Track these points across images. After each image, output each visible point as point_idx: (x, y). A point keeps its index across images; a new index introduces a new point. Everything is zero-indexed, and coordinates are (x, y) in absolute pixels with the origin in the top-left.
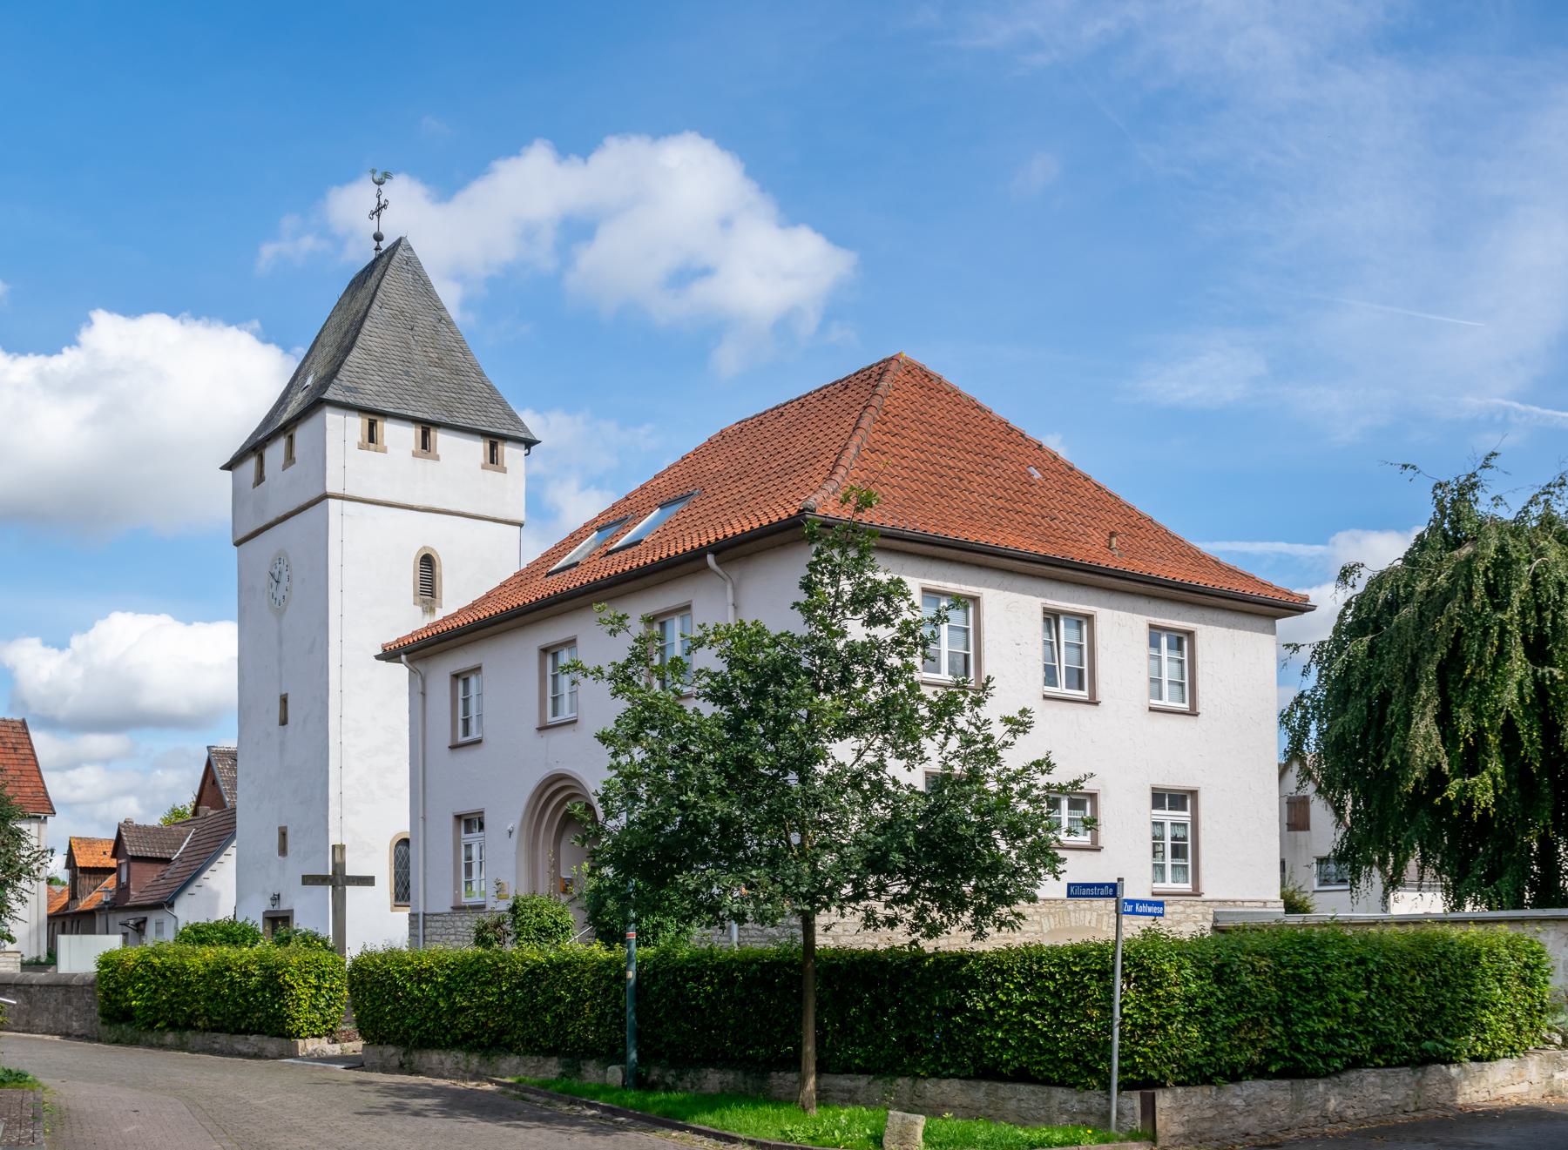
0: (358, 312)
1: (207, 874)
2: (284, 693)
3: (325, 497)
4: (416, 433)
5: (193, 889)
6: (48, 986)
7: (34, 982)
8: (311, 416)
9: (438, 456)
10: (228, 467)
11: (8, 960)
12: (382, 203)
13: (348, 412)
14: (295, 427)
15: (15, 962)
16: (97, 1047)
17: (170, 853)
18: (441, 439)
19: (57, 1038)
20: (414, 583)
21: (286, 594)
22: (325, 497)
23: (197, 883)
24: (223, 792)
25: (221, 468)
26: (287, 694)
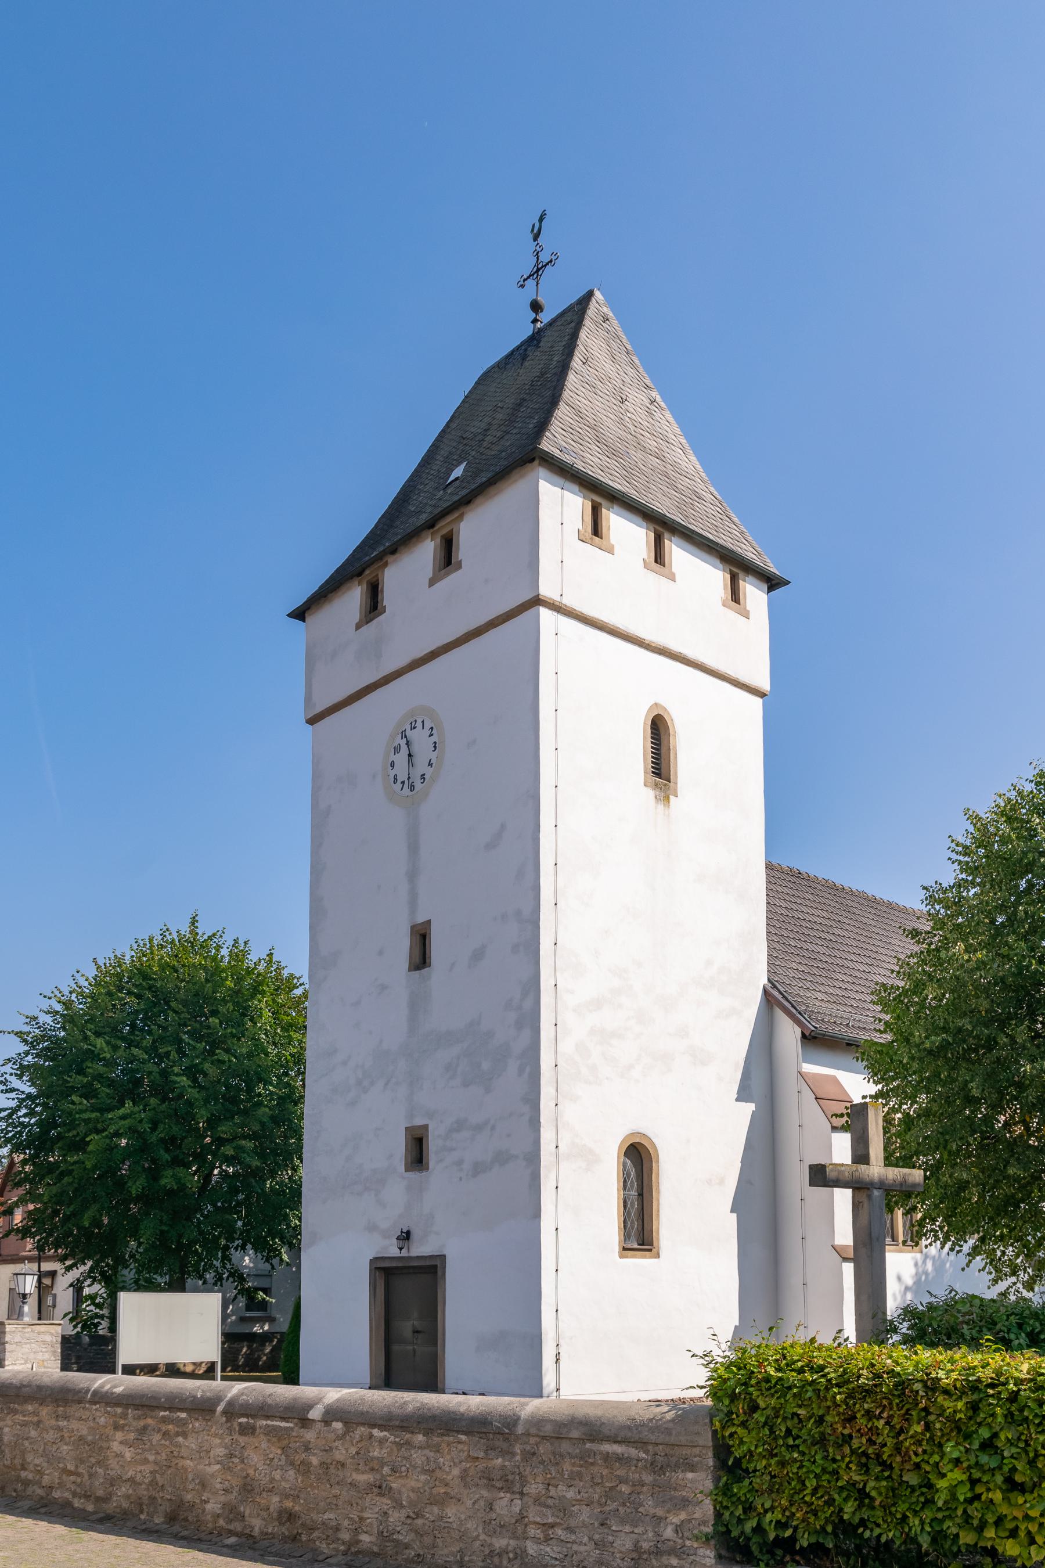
2: (421, 919)
3: (537, 601)
9: (674, 575)
10: (300, 614)
13: (568, 484)
18: (677, 552)
21: (429, 772)
22: (537, 601)
26: (429, 922)
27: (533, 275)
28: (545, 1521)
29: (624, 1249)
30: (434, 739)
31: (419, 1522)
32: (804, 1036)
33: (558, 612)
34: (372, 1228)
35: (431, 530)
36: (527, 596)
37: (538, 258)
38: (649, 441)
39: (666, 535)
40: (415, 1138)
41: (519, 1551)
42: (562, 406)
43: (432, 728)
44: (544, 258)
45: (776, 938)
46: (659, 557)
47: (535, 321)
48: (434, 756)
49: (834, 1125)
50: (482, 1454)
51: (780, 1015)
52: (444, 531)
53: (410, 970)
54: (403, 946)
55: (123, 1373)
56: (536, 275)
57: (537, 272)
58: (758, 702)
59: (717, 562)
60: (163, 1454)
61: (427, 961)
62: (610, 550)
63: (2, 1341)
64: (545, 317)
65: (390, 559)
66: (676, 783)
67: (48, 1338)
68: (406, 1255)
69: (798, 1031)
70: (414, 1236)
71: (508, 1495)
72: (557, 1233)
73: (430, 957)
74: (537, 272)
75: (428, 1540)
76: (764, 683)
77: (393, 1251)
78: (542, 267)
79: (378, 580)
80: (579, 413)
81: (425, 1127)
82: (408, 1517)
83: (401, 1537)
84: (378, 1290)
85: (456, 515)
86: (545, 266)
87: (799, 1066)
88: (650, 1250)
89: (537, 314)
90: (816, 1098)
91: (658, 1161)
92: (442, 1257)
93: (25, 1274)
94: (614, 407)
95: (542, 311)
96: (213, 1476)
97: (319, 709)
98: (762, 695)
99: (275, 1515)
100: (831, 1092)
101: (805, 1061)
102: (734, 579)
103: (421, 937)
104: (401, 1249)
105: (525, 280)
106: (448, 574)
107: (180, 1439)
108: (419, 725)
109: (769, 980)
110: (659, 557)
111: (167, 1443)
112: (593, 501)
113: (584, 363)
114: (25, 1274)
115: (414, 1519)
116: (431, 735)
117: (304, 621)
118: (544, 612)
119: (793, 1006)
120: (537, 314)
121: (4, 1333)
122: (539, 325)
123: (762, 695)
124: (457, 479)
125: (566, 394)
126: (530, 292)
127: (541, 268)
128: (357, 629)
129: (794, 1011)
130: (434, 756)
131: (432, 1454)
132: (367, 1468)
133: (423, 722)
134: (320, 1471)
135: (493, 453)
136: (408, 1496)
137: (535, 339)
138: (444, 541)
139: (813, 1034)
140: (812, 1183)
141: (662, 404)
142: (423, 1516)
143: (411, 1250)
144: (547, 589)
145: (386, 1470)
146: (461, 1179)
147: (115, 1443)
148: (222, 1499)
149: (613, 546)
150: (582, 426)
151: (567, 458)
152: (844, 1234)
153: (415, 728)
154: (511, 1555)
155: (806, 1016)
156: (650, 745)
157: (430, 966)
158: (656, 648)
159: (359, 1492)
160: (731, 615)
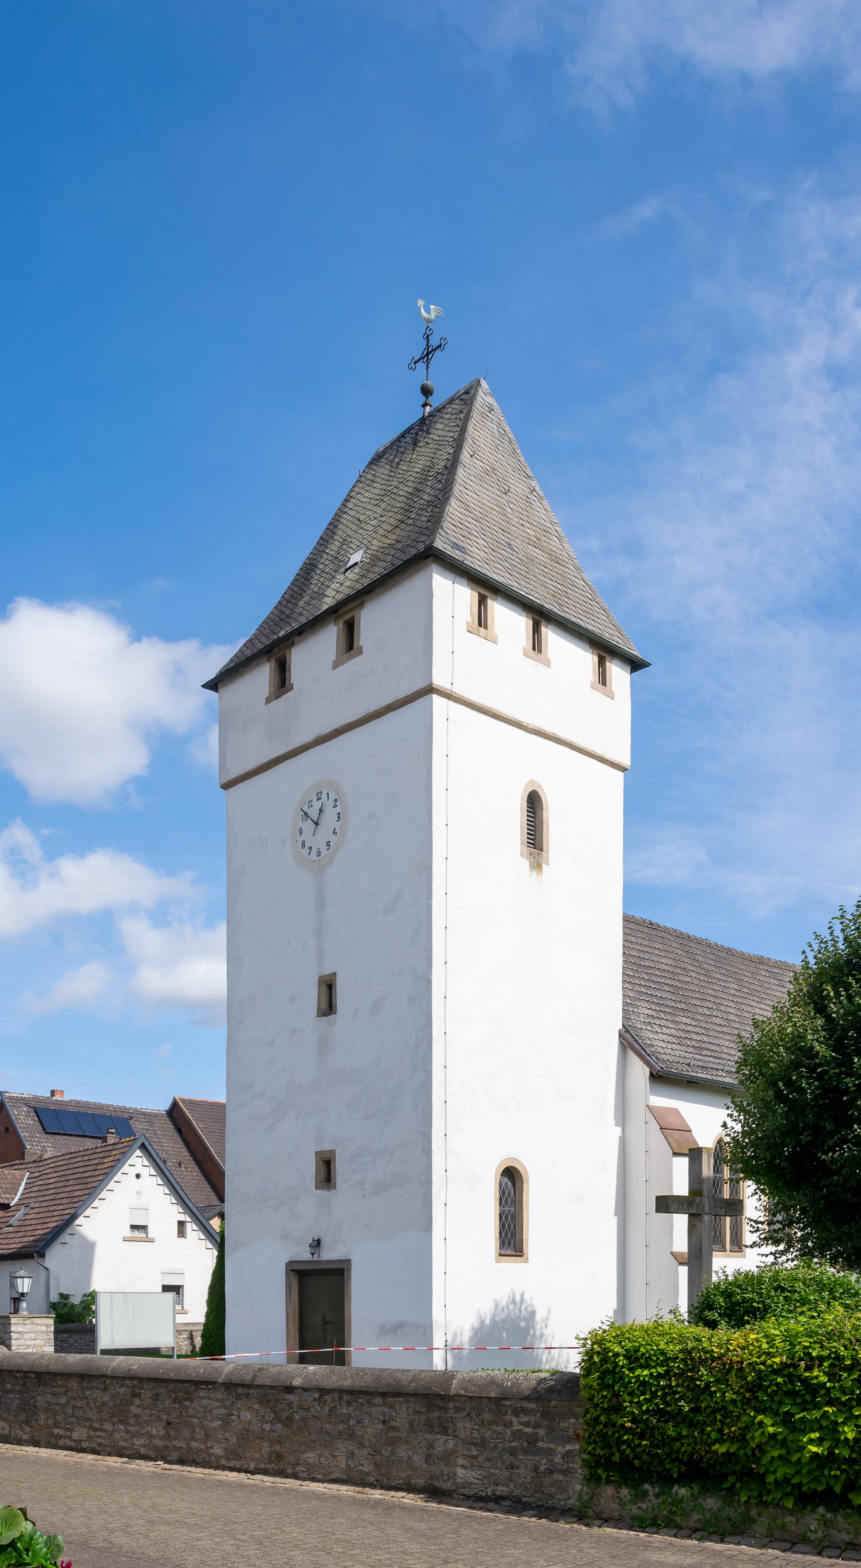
0: (422, 481)
1: (79, 1221)
2: (328, 971)
3: (430, 690)
4: (527, 622)
5: (65, 1237)
6: (351, 1392)
7: (297, 1382)
8: (397, 584)
9: (549, 661)
10: (213, 685)
11: (38, 1328)
12: (421, 366)
13: (458, 579)
14: (362, 605)
15: (47, 1332)
16: (753, 1559)
17: (7, 1198)
18: (551, 636)
19: (409, 1499)
20: (521, 827)
21: (334, 839)
22: (430, 690)
23: (69, 1230)
24: (24, 1139)
25: (204, 686)
26: (335, 974)
27: (423, 358)
28: (471, 1454)
29: (500, 1255)
30: (338, 810)
31: (378, 1457)
32: (652, 1075)
33: (449, 699)
34: (286, 1236)
35: (335, 615)
36: (419, 684)
37: (428, 342)
38: (528, 530)
39: (543, 623)
40: (324, 1161)
41: (451, 1475)
42: (453, 502)
43: (336, 800)
44: (434, 342)
45: (627, 986)
46: (537, 645)
47: (425, 405)
48: (337, 825)
49: (675, 1151)
50: (424, 1410)
51: (634, 1059)
52: (348, 617)
53: (318, 1016)
54: (312, 995)
55: (101, 1354)
56: (426, 358)
57: (427, 355)
58: (621, 775)
59: (587, 647)
60: (174, 1415)
61: (333, 1009)
62: (494, 641)
63: (8, 1330)
64: (436, 401)
65: (297, 639)
66: (548, 853)
67: (44, 1329)
68: (317, 1259)
69: (647, 1071)
70: (324, 1243)
71: (444, 1437)
72: (446, 1243)
73: (336, 1005)
74: (427, 355)
75: (384, 1470)
76: (626, 760)
77: (306, 1256)
78: (432, 351)
79: (285, 658)
80: (467, 508)
81: (333, 1152)
82: (369, 1454)
83: (364, 1468)
84: (293, 1289)
85: (357, 602)
86: (435, 350)
87: (647, 1099)
88: (522, 1256)
89: (427, 398)
90: (661, 1128)
91: (528, 1182)
92: (348, 1262)
93: (23, 1277)
94: (498, 498)
95: (431, 395)
96: (215, 1429)
97: (232, 775)
98: (623, 769)
99: (266, 1456)
100: (674, 1123)
101: (652, 1093)
102: (601, 662)
103: (328, 986)
104: (313, 1254)
105: (415, 363)
106: (350, 658)
107: (188, 1403)
108: (324, 796)
109: (623, 1026)
110: (537, 645)
111: (177, 1406)
112: (479, 593)
113: (471, 456)
114: (23, 1277)
115: (373, 1455)
116: (335, 806)
117: (217, 691)
118: (435, 698)
119: (642, 1048)
120: (427, 398)
121: (10, 1324)
122: (428, 409)
123: (623, 769)
124: (356, 564)
125: (457, 489)
126: (419, 377)
127: (431, 352)
128: (266, 703)
129: (644, 1053)
130: (337, 825)
131: (386, 1410)
132: (337, 1421)
133: (328, 794)
134: (301, 1424)
135: (389, 542)
136: (369, 1440)
137: (424, 424)
138: (346, 626)
139: (659, 1073)
140: (658, 1210)
141: (540, 492)
142: (381, 1453)
143: (321, 1255)
144: (438, 680)
145: (352, 1422)
146: (364, 1196)
147: (133, 1407)
148: (224, 1445)
149: (497, 635)
150: (469, 520)
151: (457, 555)
152: (681, 1243)
153: (320, 799)
154: (446, 1478)
155: (654, 1058)
156: (525, 808)
157: (336, 1013)
158: (532, 729)
159: (331, 1437)
160: (598, 696)
